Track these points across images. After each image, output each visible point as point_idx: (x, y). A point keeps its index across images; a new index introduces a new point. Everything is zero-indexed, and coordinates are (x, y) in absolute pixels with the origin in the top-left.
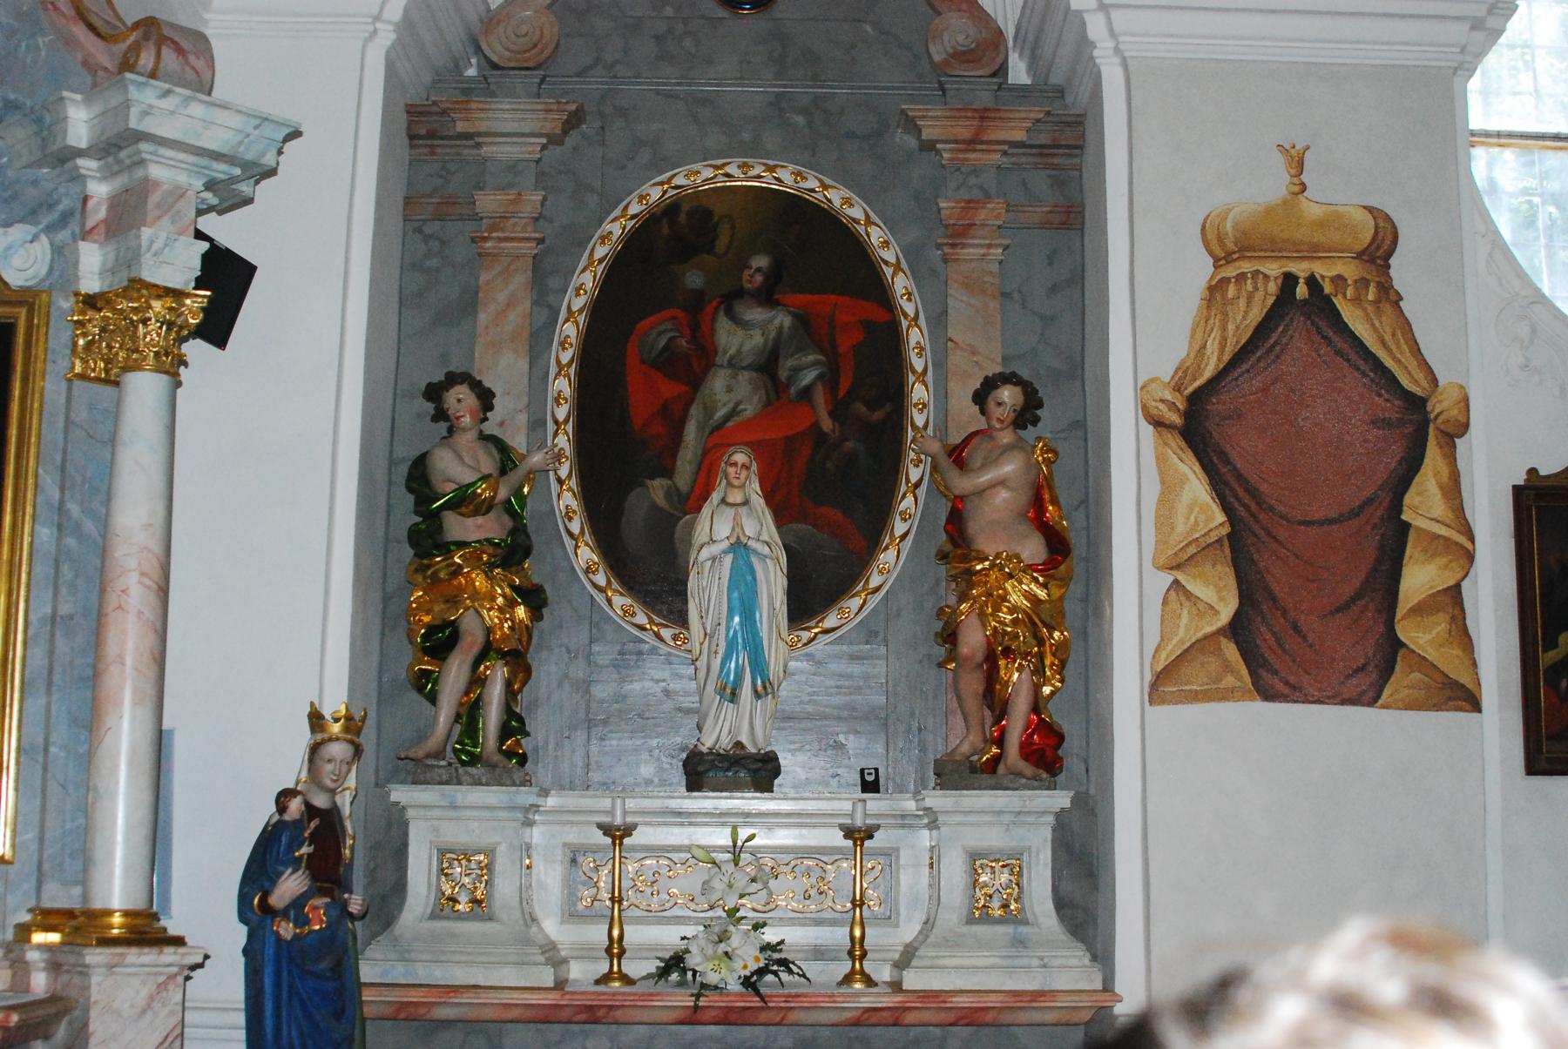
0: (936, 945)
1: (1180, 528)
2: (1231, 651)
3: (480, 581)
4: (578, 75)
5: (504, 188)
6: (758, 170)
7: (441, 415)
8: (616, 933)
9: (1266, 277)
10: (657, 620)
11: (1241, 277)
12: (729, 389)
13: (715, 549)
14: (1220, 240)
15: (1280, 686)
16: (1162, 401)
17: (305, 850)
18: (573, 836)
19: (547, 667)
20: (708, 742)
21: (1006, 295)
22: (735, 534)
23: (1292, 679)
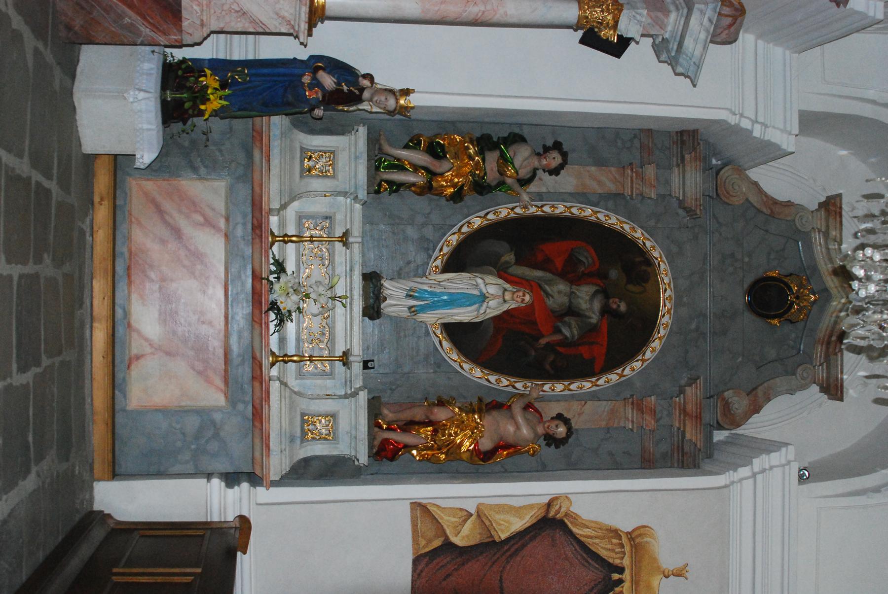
0: (290, 398)
1: (498, 517)
2: (437, 543)
3: (467, 169)
4: (714, 215)
5: (657, 179)
6: (668, 305)
7: (546, 149)
8: (294, 239)
9: (622, 558)
10: (445, 258)
11: (622, 546)
12: (559, 292)
13: (482, 286)
14: (640, 535)
15: (420, 568)
16: (560, 507)
17: (345, 88)
18: (339, 217)
19: (422, 203)
20: (386, 283)
21: (608, 430)
22: (488, 296)
23: (424, 574)
